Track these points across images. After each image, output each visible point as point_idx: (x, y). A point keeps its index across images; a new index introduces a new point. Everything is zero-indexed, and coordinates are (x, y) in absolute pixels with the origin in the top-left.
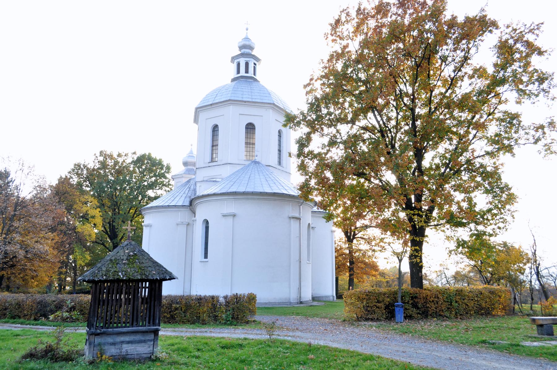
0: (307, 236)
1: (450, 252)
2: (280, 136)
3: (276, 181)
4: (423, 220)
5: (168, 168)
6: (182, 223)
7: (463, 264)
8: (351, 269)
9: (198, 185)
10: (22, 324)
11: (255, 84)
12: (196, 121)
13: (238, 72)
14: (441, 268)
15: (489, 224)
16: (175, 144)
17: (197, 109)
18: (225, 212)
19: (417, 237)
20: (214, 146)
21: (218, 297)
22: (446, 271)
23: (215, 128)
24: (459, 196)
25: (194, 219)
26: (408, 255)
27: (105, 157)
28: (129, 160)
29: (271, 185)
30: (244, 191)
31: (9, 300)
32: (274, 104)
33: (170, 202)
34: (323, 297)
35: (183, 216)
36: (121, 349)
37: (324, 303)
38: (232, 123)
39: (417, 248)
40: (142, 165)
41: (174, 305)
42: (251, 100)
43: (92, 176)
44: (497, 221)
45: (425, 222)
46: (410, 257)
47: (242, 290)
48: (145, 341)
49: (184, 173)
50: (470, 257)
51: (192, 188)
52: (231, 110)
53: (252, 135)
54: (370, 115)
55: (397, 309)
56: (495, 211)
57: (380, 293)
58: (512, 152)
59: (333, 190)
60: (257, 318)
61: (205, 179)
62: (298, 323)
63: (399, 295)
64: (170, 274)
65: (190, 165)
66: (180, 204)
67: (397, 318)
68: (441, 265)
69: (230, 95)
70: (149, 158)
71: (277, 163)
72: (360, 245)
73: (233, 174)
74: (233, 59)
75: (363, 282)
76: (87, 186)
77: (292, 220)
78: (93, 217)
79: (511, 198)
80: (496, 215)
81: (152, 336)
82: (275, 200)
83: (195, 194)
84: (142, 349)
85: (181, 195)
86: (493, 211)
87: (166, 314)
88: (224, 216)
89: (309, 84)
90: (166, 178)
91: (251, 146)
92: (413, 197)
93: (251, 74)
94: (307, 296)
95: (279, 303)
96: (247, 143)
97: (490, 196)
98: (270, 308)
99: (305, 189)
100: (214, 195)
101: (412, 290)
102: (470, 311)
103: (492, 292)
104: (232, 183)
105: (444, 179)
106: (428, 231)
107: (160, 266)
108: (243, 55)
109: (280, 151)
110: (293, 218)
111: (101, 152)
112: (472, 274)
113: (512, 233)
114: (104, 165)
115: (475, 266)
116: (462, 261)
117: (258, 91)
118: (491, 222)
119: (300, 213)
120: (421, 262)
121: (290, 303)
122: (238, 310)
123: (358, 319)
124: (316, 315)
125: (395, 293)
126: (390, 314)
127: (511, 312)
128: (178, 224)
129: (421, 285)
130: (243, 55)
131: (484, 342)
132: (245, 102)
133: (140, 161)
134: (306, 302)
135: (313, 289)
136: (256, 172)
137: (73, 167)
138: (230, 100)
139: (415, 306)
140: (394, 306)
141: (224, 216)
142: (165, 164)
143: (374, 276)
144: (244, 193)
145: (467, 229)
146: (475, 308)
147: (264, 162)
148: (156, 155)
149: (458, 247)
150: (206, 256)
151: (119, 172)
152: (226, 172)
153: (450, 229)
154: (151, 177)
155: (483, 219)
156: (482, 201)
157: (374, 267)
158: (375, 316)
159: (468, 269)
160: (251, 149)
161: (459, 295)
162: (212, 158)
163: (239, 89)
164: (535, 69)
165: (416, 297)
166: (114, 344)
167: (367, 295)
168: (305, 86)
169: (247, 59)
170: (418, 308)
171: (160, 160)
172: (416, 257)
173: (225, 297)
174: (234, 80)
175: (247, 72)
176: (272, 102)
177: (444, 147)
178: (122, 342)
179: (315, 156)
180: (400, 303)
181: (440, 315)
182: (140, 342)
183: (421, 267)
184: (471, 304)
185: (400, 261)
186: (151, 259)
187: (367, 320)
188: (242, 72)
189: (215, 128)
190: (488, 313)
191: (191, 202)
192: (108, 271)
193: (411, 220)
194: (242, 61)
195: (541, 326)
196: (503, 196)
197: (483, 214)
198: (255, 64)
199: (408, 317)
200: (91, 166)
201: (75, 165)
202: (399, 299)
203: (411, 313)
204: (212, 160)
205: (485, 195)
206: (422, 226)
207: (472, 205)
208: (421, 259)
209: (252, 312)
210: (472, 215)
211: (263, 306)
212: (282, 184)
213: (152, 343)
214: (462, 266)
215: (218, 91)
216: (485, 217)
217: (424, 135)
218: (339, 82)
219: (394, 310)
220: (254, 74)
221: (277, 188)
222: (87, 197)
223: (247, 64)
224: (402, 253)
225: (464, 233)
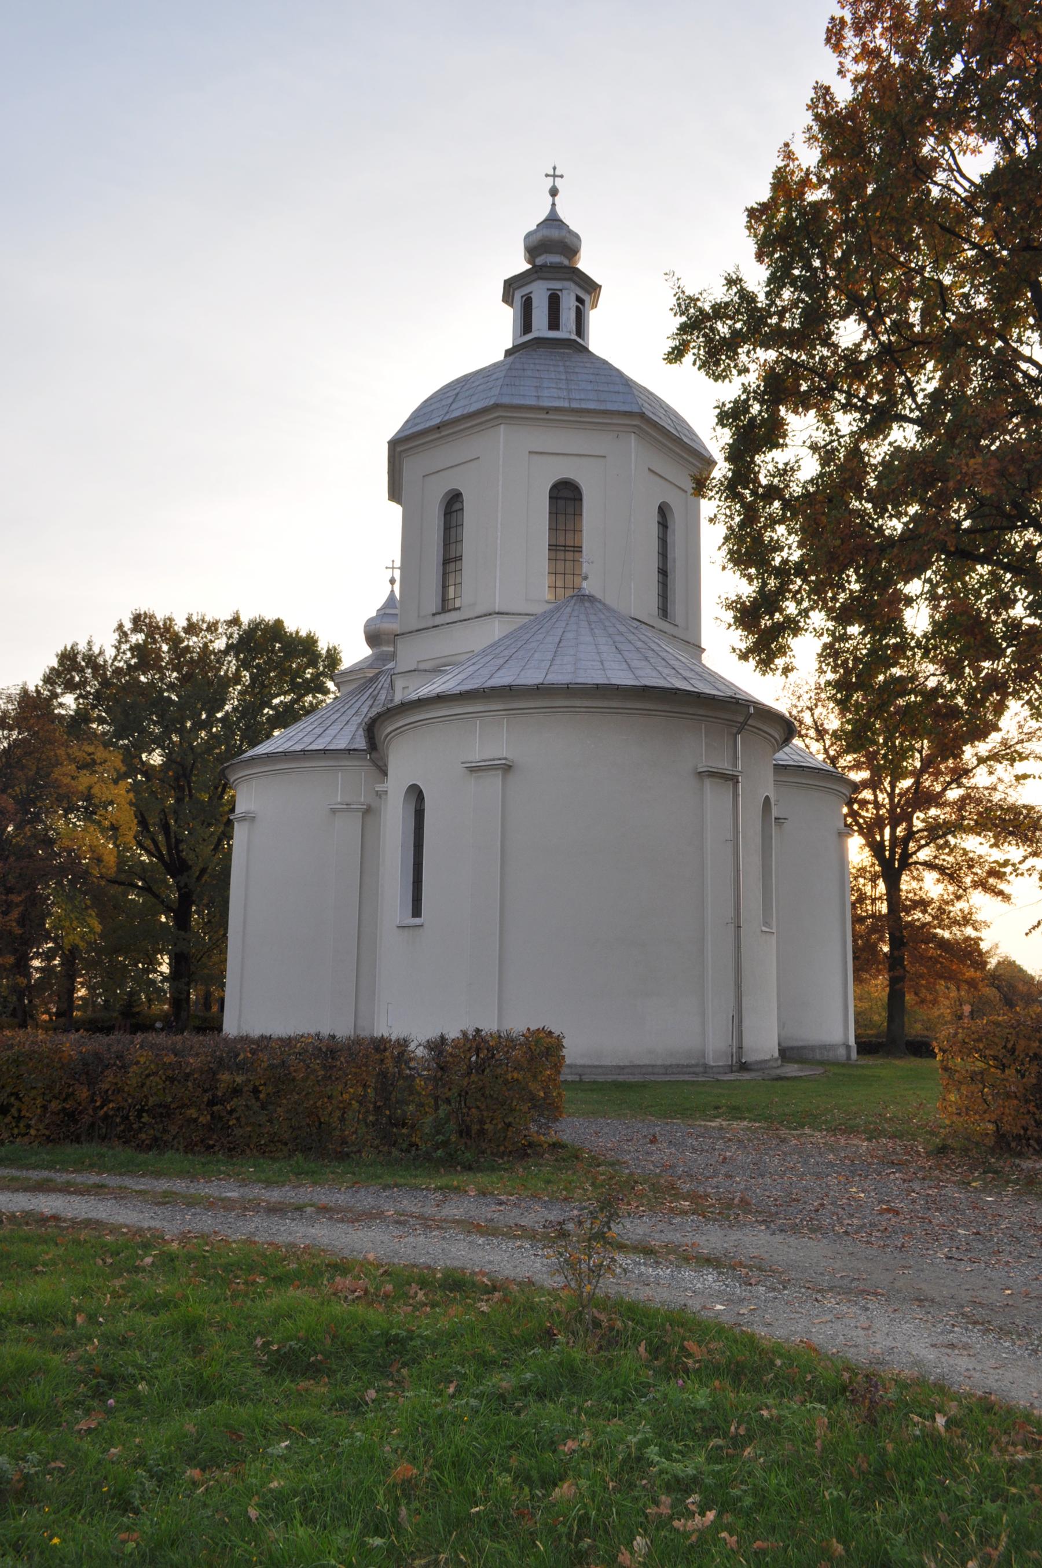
0: (759, 840)
6: (348, 808)
12: (395, 494)
17: (395, 445)
21: (403, 1044)
23: (453, 503)
25: (379, 787)
27: (150, 635)
28: (220, 644)
29: (635, 664)
30: (540, 681)
32: (642, 416)
34: (813, 1048)
37: (820, 1071)
41: (225, 1077)
42: (565, 404)
60: (571, 1129)
62: (741, 1157)
66: (342, 746)
69: (496, 391)
73: (505, 637)
75: (935, 1002)
76: (101, 721)
77: (708, 782)
85: (345, 718)
87: (193, 1113)
88: (473, 770)
91: (570, 556)
93: (567, 330)
94: (763, 1041)
95: (667, 1069)
96: (553, 547)
98: (634, 1091)
104: (501, 661)
110: (712, 774)
111: (137, 619)
114: (145, 657)
117: (592, 378)
119: (736, 758)
121: (706, 1066)
122: (477, 1108)
123: (1006, 1143)
124: (807, 1119)
128: (334, 811)
132: (547, 410)
134: (761, 1066)
135: (782, 1025)
138: (496, 406)
141: (473, 770)
142: (322, 647)
144: (540, 691)
150: (417, 912)
157: (969, 953)
160: (569, 564)
162: (444, 600)
163: (529, 373)
169: (556, 285)
173: (438, 1046)
175: (554, 323)
176: (636, 409)
191: (371, 729)
198: (580, 300)
204: (445, 606)
209: (549, 1108)
211: (610, 1078)
212: (672, 662)
221: (655, 674)
222: (90, 749)
223: (554, 302)
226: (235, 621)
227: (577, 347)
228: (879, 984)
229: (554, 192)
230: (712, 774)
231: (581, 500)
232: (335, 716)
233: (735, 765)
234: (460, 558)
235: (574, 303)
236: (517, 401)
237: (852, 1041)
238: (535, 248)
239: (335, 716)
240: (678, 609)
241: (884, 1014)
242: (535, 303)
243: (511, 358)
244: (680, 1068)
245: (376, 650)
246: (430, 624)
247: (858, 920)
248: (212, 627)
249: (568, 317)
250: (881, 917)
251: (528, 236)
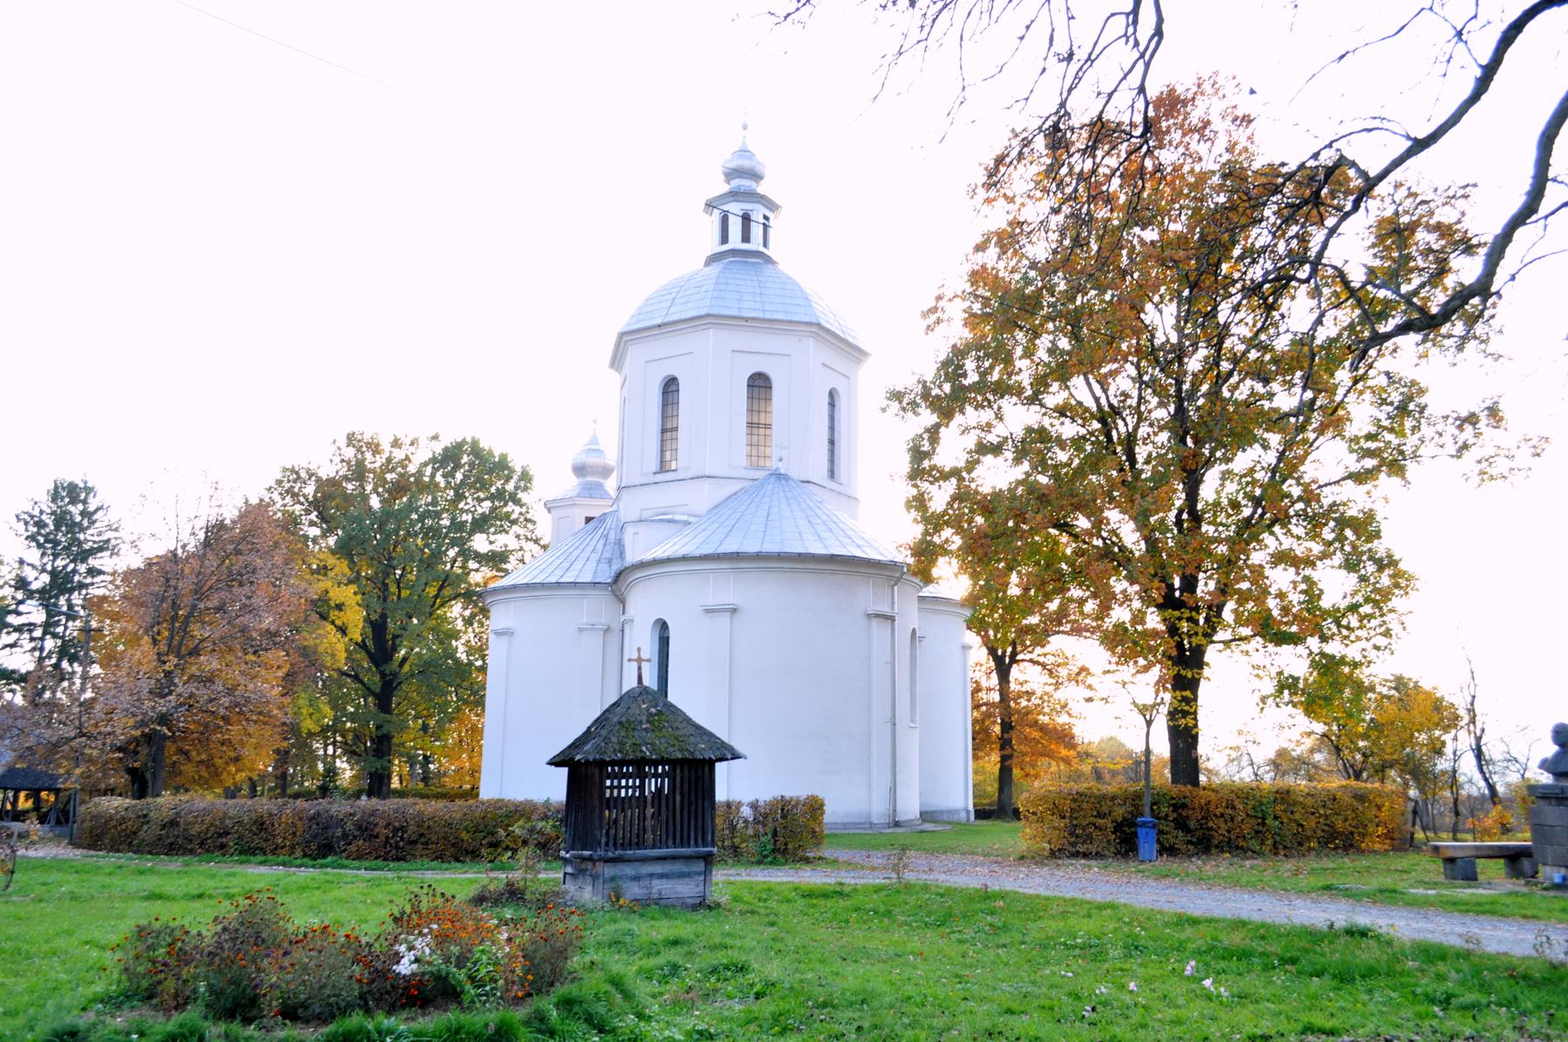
1: (1264, 699)
2: (832, 405)
3: (833, 526)
4: (1200, 631)
5: (526, 476)
7: (1295, 730)
8: (1005, 743)
9: (629, 531)
10: (284, 864)
11: (768, 269)
12: (616, 362)
13: (724, 239)
14: (1240, 741)
15: (1353, 637)
16: (553, 419)
17: (622, 335)
18: (711, 601)
19: (1185, 670)
20: (667, 431)
22: (1252, 749)
23: (670, 387)
24: (1281, 578)
26: (1164, 710)
29: (823, 535)
31: (232, 812)
32: (819, 325)
33: (559, 572)
34: (942, 812)
35: (596, 608)
36: (649, 888)
38: (713, 373)
39: (1188, 693)
40: (455, 469)
42: (760, 315)
43: (330, 501)
44: (1372, 633)
45: (1206, 635)
46: (1172, 715)
47: (796, 789)
48: (688, 875)
49: (579, 495)
50: (1310, 709)
51: (612, 536)
52: (710, 342)
53: (763, 403)
54: (1078, 382)
55: (1141, 832)
56: (1367, 609)
57: (1104, 797)
58: (1403, 478)
59: (983, 552)
60: (827, 852)
61: (646, 515)
63: (1147, 801)
64: (731, 749)
65: (592, 474)
67: (1141, 851)
68: (1240, 733)
69: (707, 302)
70: (476, 451)
71: (825, 472)
72: (1026, 676)
74: (710, 205)
76: (312, 524)
77: (874, 621)
78: (339, 607)
79: (1402, 581)
80: (1370, 617)
81: (700, 866)
82: (833, 572)
83: (622, 554)
84: (686, 889)
86: (1361, 610)
88: (709, 611)
89: (934, 310)
90: (518, 502)
91: (762, 431)
92: (1177, 583)
93: (756, 244)
94: (910, 808)
97: (1353, 578)
99: (926, 553)
100: (685, 559)
101: (1176, 790)
102: (1309, 839)
103: (1361, 797)
104: (726, 530)
105: (1248, 532)
106: (1212, 654)
107: (711, 735)
108: (735, 195)
109: (832, 442)
110: (877, 616)
111: (351, 439)
112: (1318, 757)
113: (1408, 652)
115: (1324, 735)
116: (1291, 721)
118: (1358, 632)
120: (1196, 726)
121: (872, 825)
123: (1053, 854)
125: (1137, 796)
126: (1125, 843)
127: (1403, 843)
128: (581, 630)
129: (1196, 782)
130: (735, 195)
131: (1328, 888)
132: (747, 319)
133: (450, 458)
134: (908, 823)
137: (279, 477)
139: (1181, 824)
140: (1134, 825)
141: (709, 611)
143: (1067, 761)
144: (758, 557)
145: (1300, 649)
146: (1319, 833)
147: (795, 474)
149: (1280, 691)
151: (399, 488)
152: (700, 498)
153: (1262, 651)
154: (480, 500)
155: (1339, 626)
156: (1335, 585)
157: (1064, 737)
158: (1093, 849)
159: (1309, 743)
161: (1283, 801)
162: (662, 462)
164: (1370, 516)
165: (1184, 806)
166: (637, 878)
167: (1074, 800)
168: (925, 315)
169: (747, 206)
170: (1187, 830)
171: (504, 457)
172: (1185, 714)
173: (754, 806)
174: (713, 259)
175: (746, 238)
177: (1254, 458)
178: (652, 875)
179: (945, 476)
180: (1148, 818)
181: (1237, 848)
182: (681, 875)
183: (1195, 738)
184: (1310, 823)
185: (1149, 723)
186: (689, 721)
187: (1076, 855)
188: (735, 240)
189: (670, 387)
190: (1351, 846)
192: (622, 743)
193: (1173, 630)
195: (1451, 861)
196: (1382, 581)
197: (1337, 616)
198: (766, 218)
199: (1168, 850)
200: (327, 471)
201: (285, 470)
202: (1147, 810)
203: (1172, 841)
204: (663, 467)
205: (1344, 572)
206: (1199, 646)
207: (1312, 593)
208: (1195, 719)
209: (817, 837)
210: (1314, 618)
214: (1295, 734)
215: (674, 291)
216: (1344, 622)
217: (1205, 430)
218: (1007, 310)
219: (1135, 834)
220: (765, 245)
223: (746, 219)
224: (1153, 706)
225: (1295, 661)
228: (993, 761)
230: (877, 616)
232: (576, 553)
236: (725, 312)
237: (971, 807)
240: (842, 470)
241: (996, 786)
243: (716, 268)
244: (855, 825)
247: (976, 707)
249: (756, 231)
250: (992, 705)
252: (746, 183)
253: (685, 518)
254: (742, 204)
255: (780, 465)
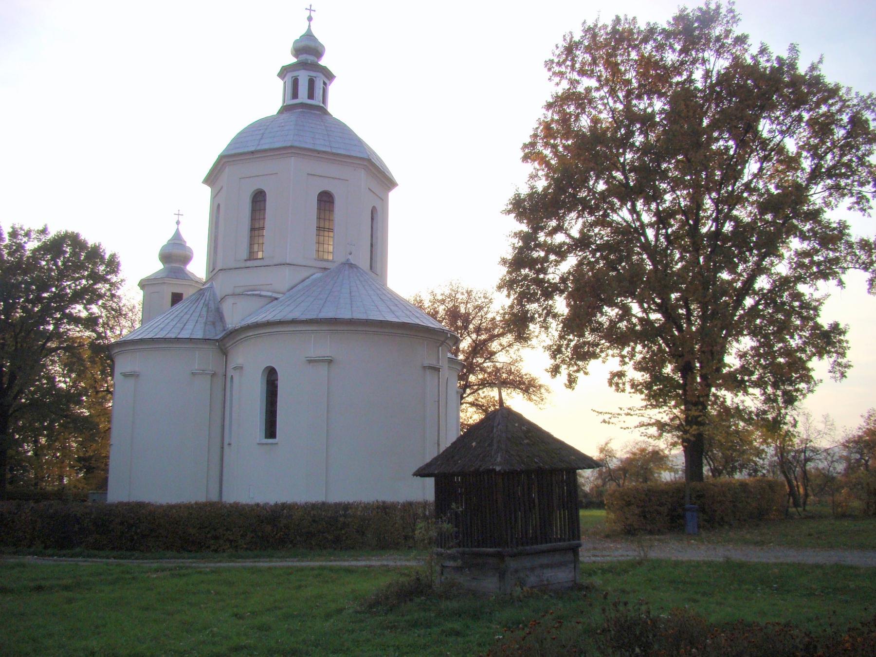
11: (326, 116)
13: (295, 95)
20: (256, 229)
23: (259, 199)
29: (393, 308)
32: (369, 161)
33: (165, 333)
42: (328, 150)
49: (167, 277)
52: (292, 168)
61: (238, 291)
66: (173, 336)
70: (74, 240)
77: (428, 372)
81: (570, 556)
84: (562, 576)
88: (311, 361)
91: (326, 233)
96: (319, 228)
100: (294, 322)
109: (372, 245)
132: (319, 152)
133: (54, 247)
136: (358, 282)
138: (291, 147)
148: (90, 238)
150: (271, 431)
169: (313, 74)
175: (311, 96)
188: (303, 97)
189: (259, 199)
194: (303, 77)
204: (251, 256)
213: (572, 566)
223: (311, 83)
226: (44, 231)
227: (322, 111)
229: (310, 19)
231: (333, 203)
232: (187, 317)
233: (438, 363)
234: (263, 228)
235: (322, 85)
238: (298, 50)
239: (187, 317)
242: (301, 82)
243: (285, 116)
245: (166, 265)
246: (243, 265)
248: (28, 234)
249: (318, 92)
251: (296, 42)
252: (311, 58)
253: (270, 294)
254: (307, 70)
255: (350, 257)
